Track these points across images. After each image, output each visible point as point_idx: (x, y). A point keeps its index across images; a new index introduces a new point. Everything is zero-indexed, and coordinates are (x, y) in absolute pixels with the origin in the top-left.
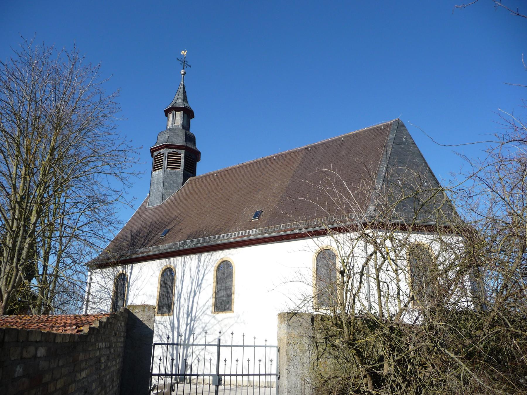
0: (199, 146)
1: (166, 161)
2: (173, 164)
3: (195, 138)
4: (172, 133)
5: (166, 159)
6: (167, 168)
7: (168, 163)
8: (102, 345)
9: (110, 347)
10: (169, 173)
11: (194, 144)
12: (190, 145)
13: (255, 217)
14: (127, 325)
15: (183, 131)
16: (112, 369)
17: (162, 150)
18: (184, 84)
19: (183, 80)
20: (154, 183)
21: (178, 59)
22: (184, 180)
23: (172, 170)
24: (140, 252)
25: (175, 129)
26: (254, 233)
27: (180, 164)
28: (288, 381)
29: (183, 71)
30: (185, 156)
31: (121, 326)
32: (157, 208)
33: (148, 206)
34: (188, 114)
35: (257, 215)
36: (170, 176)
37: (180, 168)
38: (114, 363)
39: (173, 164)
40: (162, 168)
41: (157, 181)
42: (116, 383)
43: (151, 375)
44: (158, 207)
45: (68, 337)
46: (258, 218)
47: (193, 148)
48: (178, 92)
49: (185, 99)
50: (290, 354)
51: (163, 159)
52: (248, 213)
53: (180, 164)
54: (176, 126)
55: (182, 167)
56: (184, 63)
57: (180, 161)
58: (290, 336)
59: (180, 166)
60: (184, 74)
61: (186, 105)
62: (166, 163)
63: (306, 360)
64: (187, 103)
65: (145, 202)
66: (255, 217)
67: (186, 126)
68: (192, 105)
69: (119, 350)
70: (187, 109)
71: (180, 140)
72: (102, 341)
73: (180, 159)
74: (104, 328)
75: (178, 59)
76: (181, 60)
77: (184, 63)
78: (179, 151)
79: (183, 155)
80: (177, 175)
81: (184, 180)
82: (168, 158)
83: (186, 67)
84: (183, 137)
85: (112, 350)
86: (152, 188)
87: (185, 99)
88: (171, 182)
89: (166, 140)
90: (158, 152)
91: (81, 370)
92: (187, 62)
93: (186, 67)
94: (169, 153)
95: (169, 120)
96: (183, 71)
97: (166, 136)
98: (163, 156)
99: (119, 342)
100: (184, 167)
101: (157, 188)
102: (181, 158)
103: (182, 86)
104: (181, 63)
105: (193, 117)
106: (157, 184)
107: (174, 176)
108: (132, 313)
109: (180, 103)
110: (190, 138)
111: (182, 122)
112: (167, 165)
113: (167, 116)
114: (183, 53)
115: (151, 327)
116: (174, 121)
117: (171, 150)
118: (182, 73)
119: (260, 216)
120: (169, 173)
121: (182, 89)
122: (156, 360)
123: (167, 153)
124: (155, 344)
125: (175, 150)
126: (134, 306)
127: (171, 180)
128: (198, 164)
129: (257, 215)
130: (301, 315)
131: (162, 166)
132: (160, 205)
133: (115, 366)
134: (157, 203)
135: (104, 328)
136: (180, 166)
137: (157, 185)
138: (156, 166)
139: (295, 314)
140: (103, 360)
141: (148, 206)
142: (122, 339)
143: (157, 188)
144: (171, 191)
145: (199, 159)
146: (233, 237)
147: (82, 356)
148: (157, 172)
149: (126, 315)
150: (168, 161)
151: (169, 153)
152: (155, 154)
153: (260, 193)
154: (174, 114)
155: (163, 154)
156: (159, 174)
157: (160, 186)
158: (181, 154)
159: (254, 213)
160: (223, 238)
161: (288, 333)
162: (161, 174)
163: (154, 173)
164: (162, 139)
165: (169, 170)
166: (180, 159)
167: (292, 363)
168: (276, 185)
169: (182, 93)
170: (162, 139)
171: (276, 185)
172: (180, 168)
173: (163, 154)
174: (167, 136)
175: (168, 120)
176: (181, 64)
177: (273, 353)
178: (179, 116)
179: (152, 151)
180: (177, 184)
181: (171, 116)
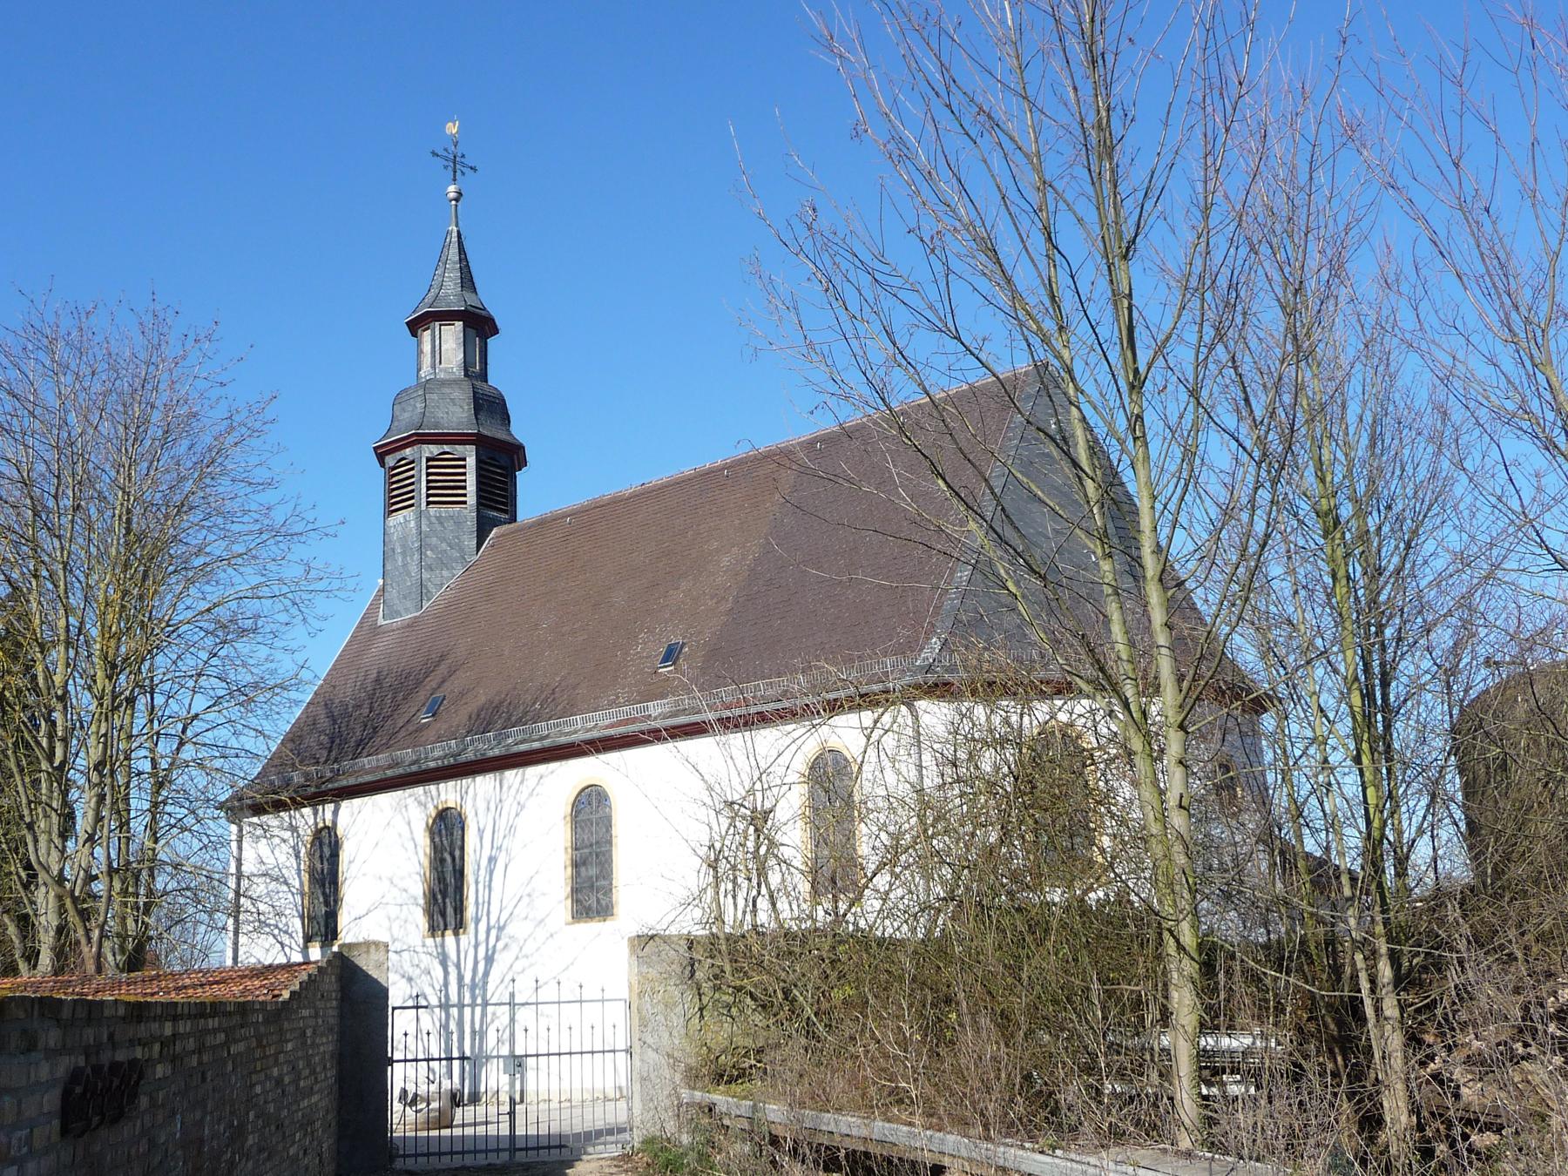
0: (520, 431)
1: (424, 484)
2: (444, 489)
3: (504, 401)
4: (435, 397)
5: (424, 478)
6: (428, 503)
7: (428, 488)
8: (305, 1013)
9: (316, 1016)
10: (433, 520)
11: (506, 419)
12: (491, 430)
13: (665, 660)
14: (340, 979)
15: (467, 386)
16: (322, 1049)
17: (408, 451)
18: (459, 232)
19: (457, 217)
20: (393, 550)
21: (434, 154)
22: (481, 538)
23: (443, 509)
24: (371, 764)
25: (443, 383)
26: (657, 711)
27: (464, 488)
28: (642, 1060)
29: (452, 188)
30: (479, 461)
31: (330, 982)
32: (408, 626)
33: (381, 622)
34: (479, 325)
35: (671, 655)
36: (439, 528)
37: (465, 503)
38: (324, 1040)
39: (444, 489)
40: (412, 505)
41: (403, 546)
42: (331, 1073)
43: (391, 1062)
44: (411, 625)
45: (193, 1007)
46: (674, 664)
47: (501, 435)
48: (444, 258)
49: (467, 281)
50: (644, 1012)
51: (413, 476)
52: (649, 647)
53: (464, 488)
54: (445, 370)
55: (471, 499)
56: (454, 163)
57: (465, 481)
58: (643, 978)
59: (465, 495)
60: (457, 200)
61: (471, 300)
62: (424, 490)
63: (677, 1021)
64: (474, 290)
65: (373, 607)
66: (665, 660)
67: (476, 370)
68: (491, 299)
69: (332, 1021)
70: (474, 314)
71: (456, 413)
72: (305, 1008)
73: (464, 474)
74: (306, 989)
75: (434, 154)
76: (445, 154)
77: (456, 164)
78: (459, 450)
79: (471, 462)
80: (459, 523)
81: (481, 538)
82: (428, 474)
83: (463, 173)
84: (469, 404)
85: (320, 1021)
86: (388, 567)
87: (467, 281)
88: (444, 546)
89: (416, 419)
90: (398, 455)
91: (287, 1041)
92: (463, 156)
93: (463, 173)
94: (428, 460)
95: (422, 352)
96: (452, 188)
97: (418, 405)
98: (412, 469)
99: (330, 1008)
100: (479, 497)
101: (405, 565)
102: (468, 470)
103: (455, 239)
104: (446, 163)
105: (495, 331)
106: (404, 554)
107: (450, 525)
108: (347, 958)
109: (451, 295)
110: (490, 405)
111: (462, 356)
112: (428, 496)
113: (414, 334)
114: (452, 129)
115: (382, 981)
116: (436, 352)
117: (434, 450)
118: (452, 195)
119: (678, 658)
120: (433, 520)
121: (454, 250)
122: (398, 1035)
123: (424, 460)
124: (394, 1009)
125: (446, 448)
126: (350, 946)
127: (443, 540)
128: (521, 477)
129: (671, 655)
130: (666, 940)
131: (412, 498)
132: (415, 617)
133: (326, 1045)
134: (407, 610)
135: (306, 989)
136: (465, 495)
137: (404, 557)
138: (396, 498)
139: (652, 937)
140: (309, 1033)
141: (381, 622)
142: (334, 1003)
143: (405, 565)
144: (445, 573)
145: (523, 463)
146: (607, 722)
147: (286, 1025)
148: (399, 517)
149: (338, 963)
150: (428, 482)
151: (428, 460)
152: (390, 460)
153: (684, 585)
154: (437, 333)
155: (413, 462)
156: (403, 519)
157: (412, 559)
158: (464, 460)
159: (663, 650)
160: (580, 727)
161: (640, 973)
162: (413, 524)
163: (392, 521)
164: (406, 415)
165: (433, 510)
166: (464, 474)
167: (650, 1029)
168: (725, 561)
169: (455, 263)
170: (406, 415)
171: (725, 561)
172: (465, 503)
173: (413, 462)
174: (420, 406)
175: (420, 352)
176: (446, 167)
177: (617, 1014)
178: (451, 336)
179: (381, 454)
180: (461, 550)
181: (427, 335)
